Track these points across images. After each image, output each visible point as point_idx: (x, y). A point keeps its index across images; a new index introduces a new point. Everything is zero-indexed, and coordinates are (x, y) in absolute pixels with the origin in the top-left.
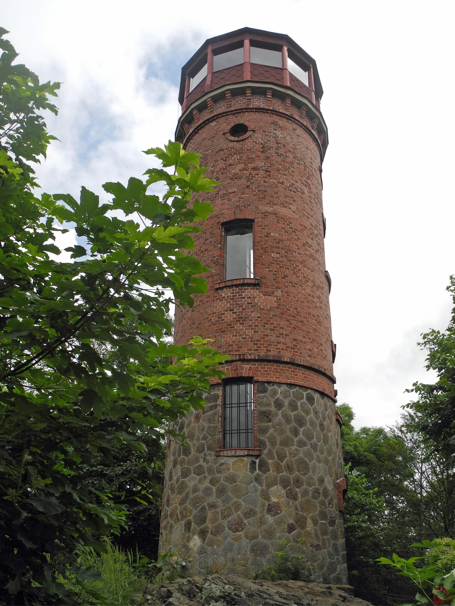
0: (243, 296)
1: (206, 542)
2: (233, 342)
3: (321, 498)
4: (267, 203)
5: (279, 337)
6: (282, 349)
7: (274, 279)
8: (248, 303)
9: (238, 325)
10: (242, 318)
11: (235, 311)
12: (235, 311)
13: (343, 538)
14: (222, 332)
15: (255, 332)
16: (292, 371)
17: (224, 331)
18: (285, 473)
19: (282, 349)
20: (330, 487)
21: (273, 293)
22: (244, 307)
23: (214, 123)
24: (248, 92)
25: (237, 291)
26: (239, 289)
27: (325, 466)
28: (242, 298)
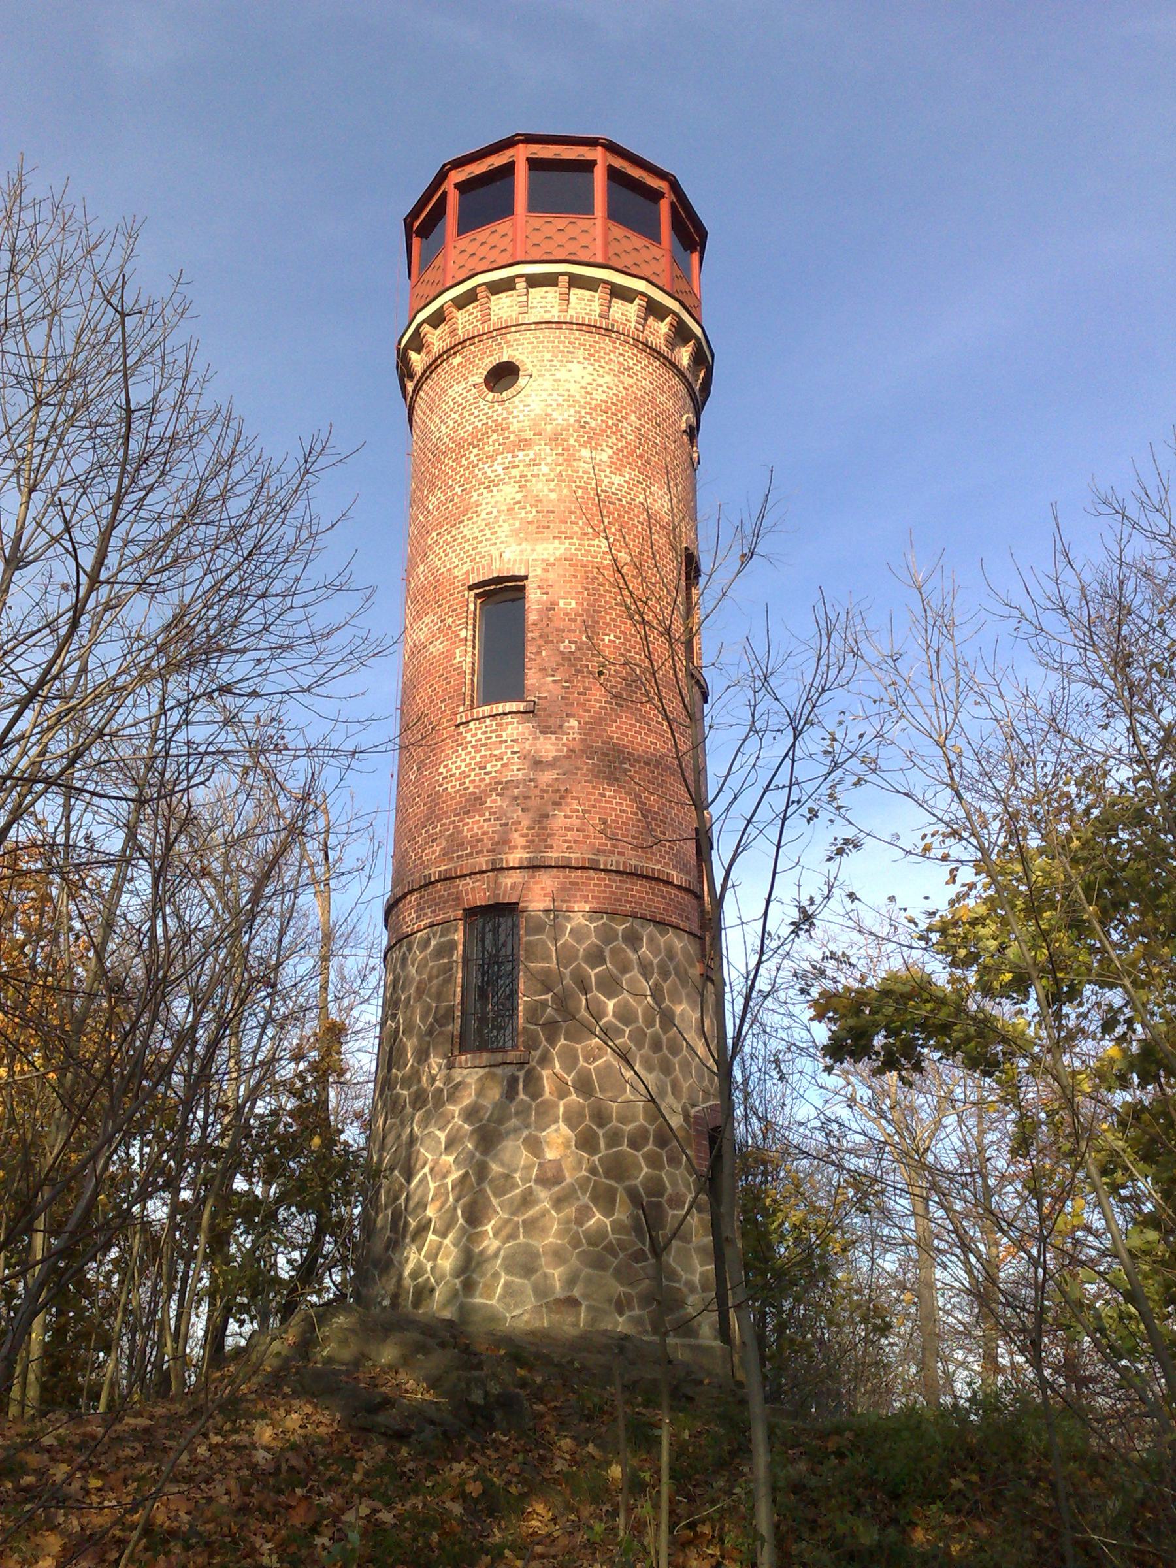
0: (504, 738)
1: (423, 1253)
2: (484, 833)
3: (650, 1147)
4: (554, 538)
5: (548, 571)
6: (575, 842)
7: (562, 698)
8: (513, 753)
9: (494, 797)
10: (501, 783)
11: (489, 769)
12: (489, 769)
13: (708, 1235)
14: (465, 813)
15: (523, 810)
16: (595, 885)
17: (469, 812)
18: (574, 1097)
19: (575, 842)
20: (676, 1121)
21: (561, 727)
22: (505, 761)
23: (457, 360)
24: (521, 284)
25: (494, 727)
26: (497, 724)
27: (662, 1076)
28: (501, 742)
